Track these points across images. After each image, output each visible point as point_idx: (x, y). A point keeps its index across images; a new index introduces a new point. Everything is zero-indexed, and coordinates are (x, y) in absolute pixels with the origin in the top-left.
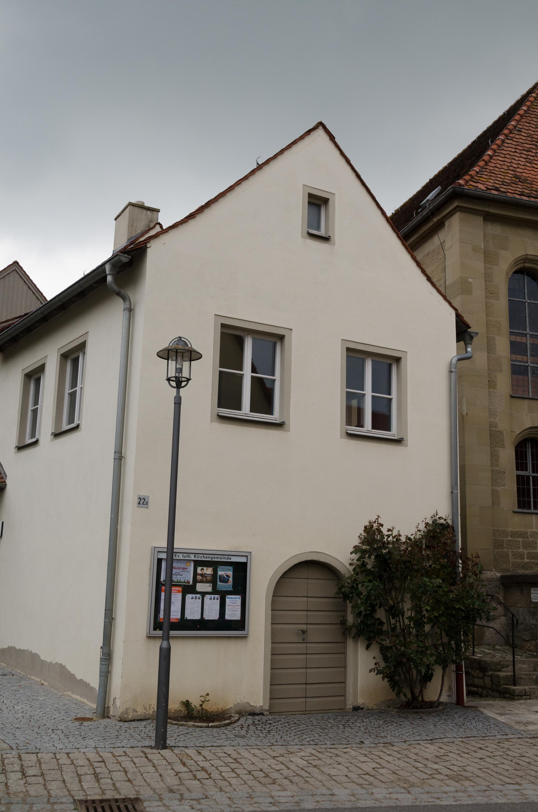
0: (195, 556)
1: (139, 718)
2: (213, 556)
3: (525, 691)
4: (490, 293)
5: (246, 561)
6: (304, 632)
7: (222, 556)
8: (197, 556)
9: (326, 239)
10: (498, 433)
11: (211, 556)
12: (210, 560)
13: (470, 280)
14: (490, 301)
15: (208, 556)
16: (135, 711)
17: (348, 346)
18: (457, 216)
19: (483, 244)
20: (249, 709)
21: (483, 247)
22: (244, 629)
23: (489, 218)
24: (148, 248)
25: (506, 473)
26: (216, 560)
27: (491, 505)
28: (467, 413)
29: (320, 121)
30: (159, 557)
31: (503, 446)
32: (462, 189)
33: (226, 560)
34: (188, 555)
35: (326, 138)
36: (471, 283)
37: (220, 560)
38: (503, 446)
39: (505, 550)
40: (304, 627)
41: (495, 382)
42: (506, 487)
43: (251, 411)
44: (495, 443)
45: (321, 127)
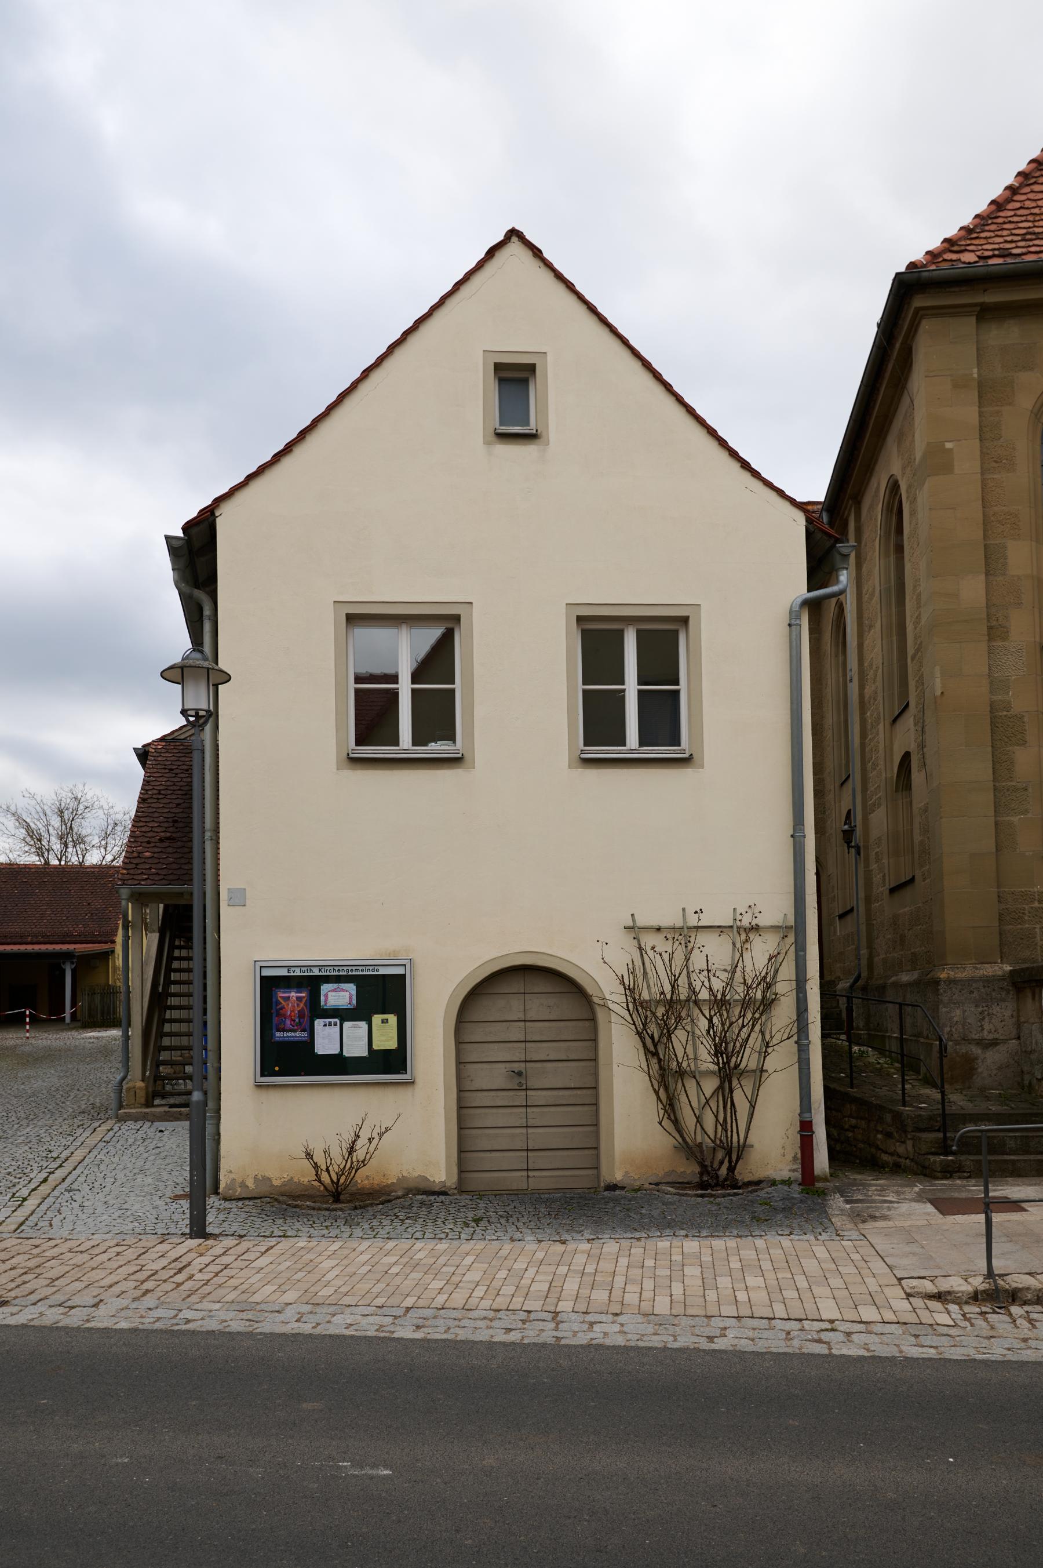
0: (320, 970)
1: (250, 1196)
2: (350, 968)
3: (960, 1164)
4: (996, 462)
5: (403, 973)
6: (519, 1074)
7: (364, 968)
8: (323, 970)
9: (531, 437)
10: (1012, 720)
11: (345, 968)
12: (345, 974)
13: (948, 445)
14: (995, 476)
15: (341, 968)
16: (243, 1184)
17: (580, 614)
18: (926, 325)
19: (975, 370)
20: (423, 1185)
21: (975, 375)
22: (406, 1071)
23: (986, 314)
24: (217, 517)
25: (1030, 790)
26: (354, 973)
27: (994, 850)
28: (942, 693)
29: (510, 228)
30: (263, 974)
31: (1023, 743)
32: (916, 275)
33: (371, 973)
34: (309, 968)
35: (526, 255)
36: (951, 450)
37: (361, 973)
38: (1023, 743)
39: (1027, 926)
40: (517, 1067)
41: (1004, 627)
42: (1029, 815)
43: (413, 745)
44: (1006, 740)
45: (514, 239)
